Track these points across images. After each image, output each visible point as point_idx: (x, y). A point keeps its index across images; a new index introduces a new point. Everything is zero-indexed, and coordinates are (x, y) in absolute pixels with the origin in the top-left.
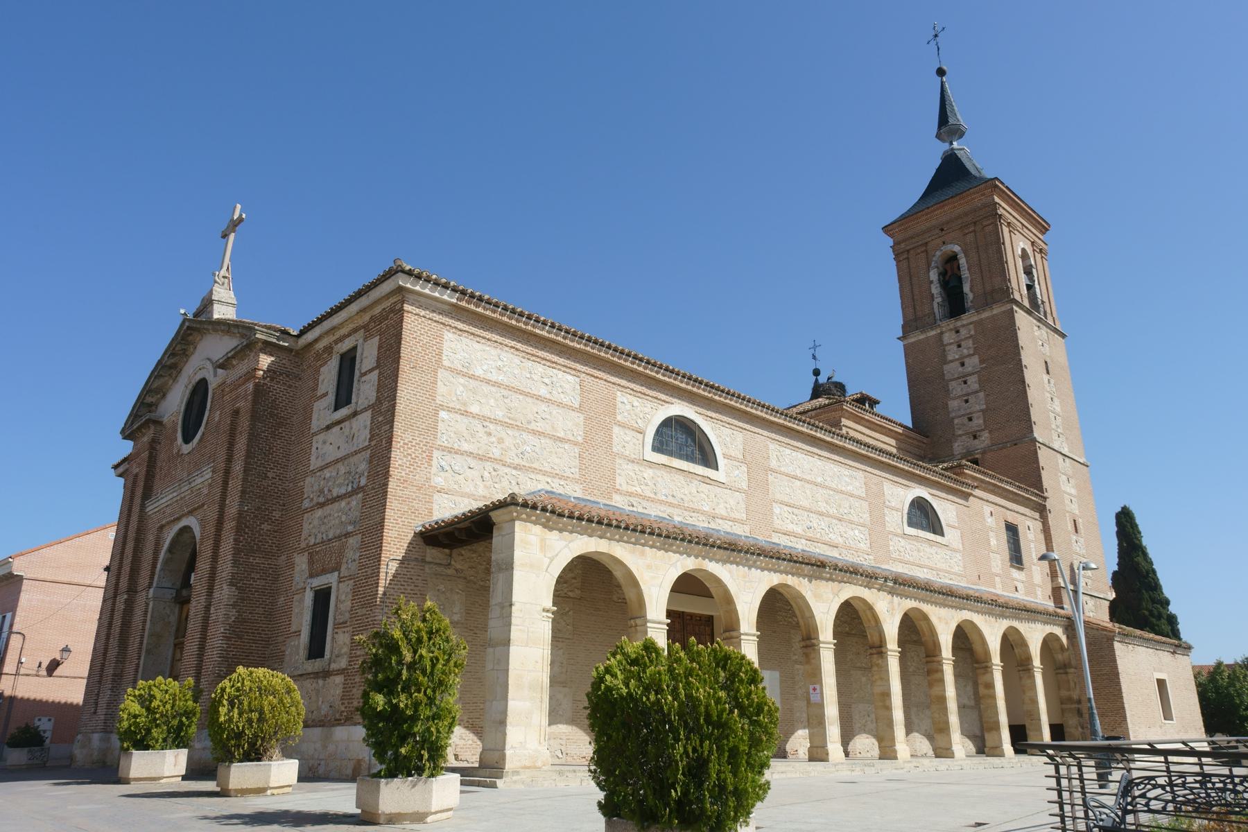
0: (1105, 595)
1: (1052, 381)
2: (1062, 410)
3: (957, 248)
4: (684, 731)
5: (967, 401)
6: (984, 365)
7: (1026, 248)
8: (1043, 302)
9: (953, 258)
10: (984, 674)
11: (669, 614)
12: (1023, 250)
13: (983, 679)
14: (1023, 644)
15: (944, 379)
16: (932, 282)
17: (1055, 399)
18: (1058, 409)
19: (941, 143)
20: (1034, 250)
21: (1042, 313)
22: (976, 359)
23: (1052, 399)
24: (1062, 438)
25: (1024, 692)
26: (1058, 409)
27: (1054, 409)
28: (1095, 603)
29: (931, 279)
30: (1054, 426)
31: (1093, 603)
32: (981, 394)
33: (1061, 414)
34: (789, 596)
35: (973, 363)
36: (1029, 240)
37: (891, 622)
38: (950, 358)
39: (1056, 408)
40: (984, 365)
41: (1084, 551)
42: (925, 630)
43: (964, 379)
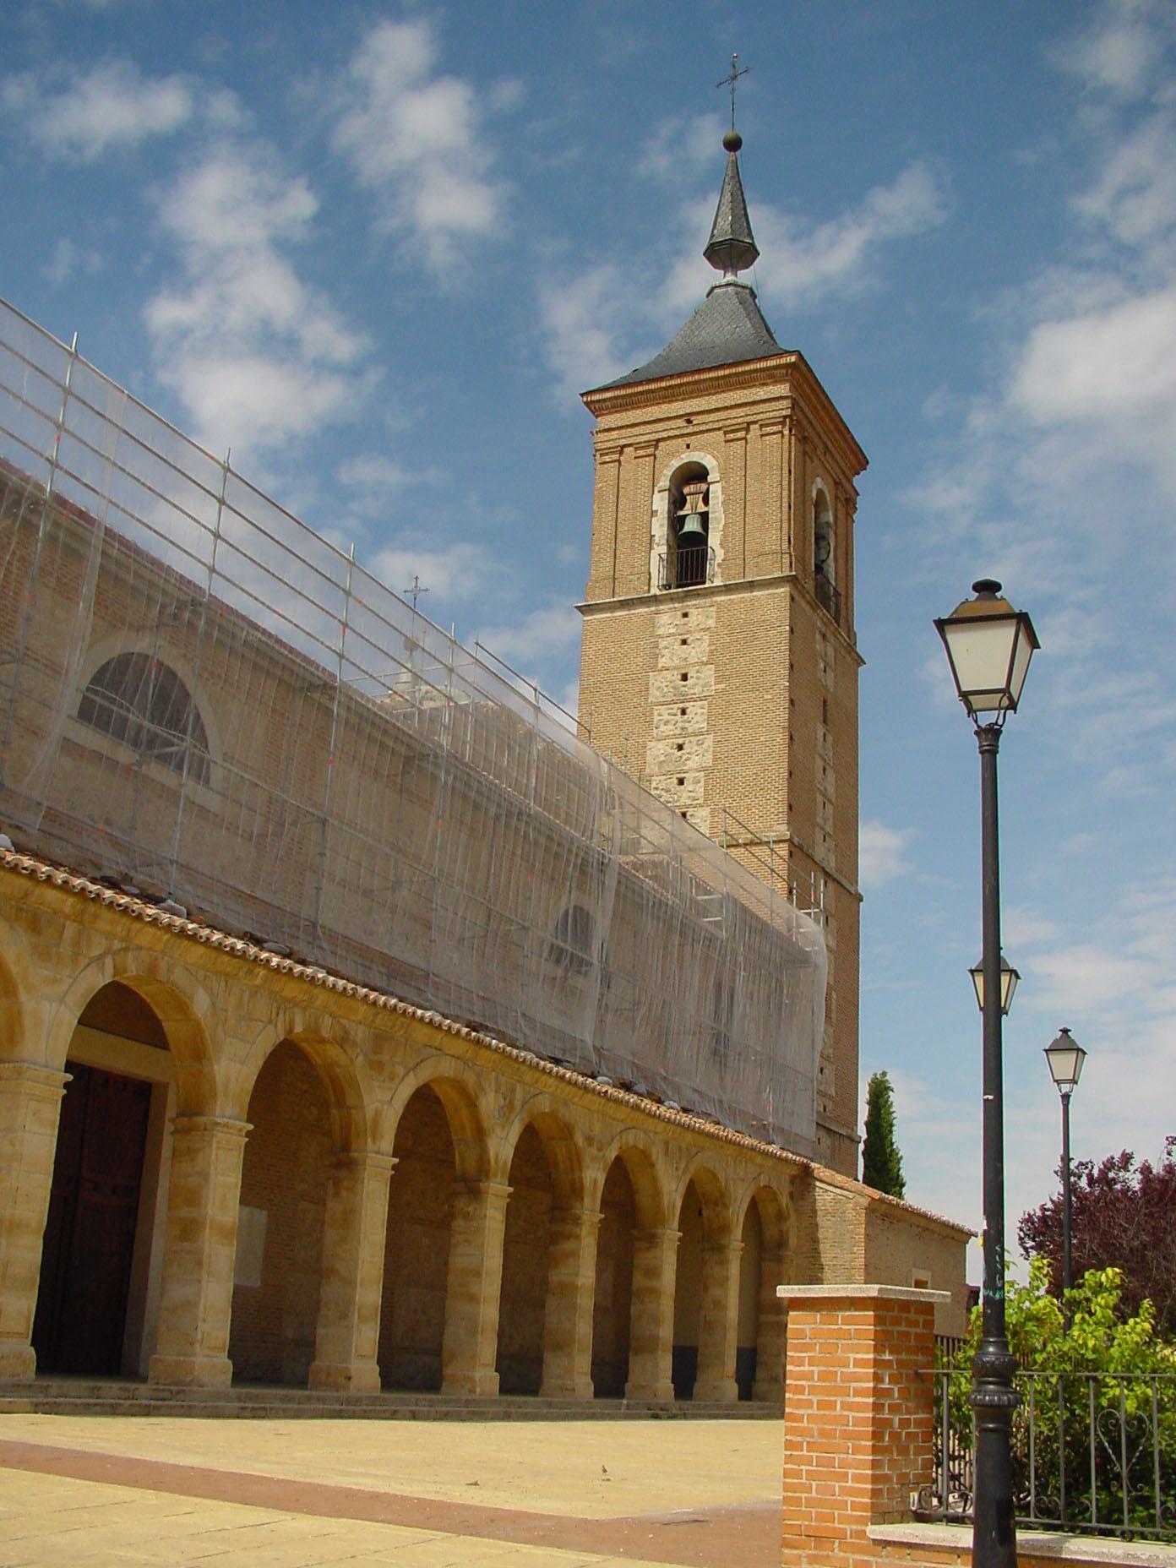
0: (850, 1131)
1: (830, 738)
2: (836, 793)
3: (709, 462)
4: (45, 523)
5: (680, 747)
6: (723, 686)
7: (826, 491)
8: (837, 594)
9: (695, 474)
10: (648, 1249)
11: (70, 1066)
12: (820, 492)
13: (643, 1259)
14: (720, 1200)
15: (717, 665)
16: (653, 513)
17: (829, 772)
18: (831, 790)
19: (711, 267)
20: (837, 497)
21: (832, 612)
22: (709, 671)
23: (824, 769)
24: (831, 843)
25: (706, 1288)
26: (831, 790)
27: (825, 789)
28: (833, 1143)
29: (654, 509)
30: (819, 820)
31: (829, 1143)
32: (709, 740)
33: (833, 800)
34: (317, 1059)
35: (704, 680)
36: (832, 476)
37: (504, 1135)
38: (662, 662)
39: (829, 788)
40: (723, 686)
41: (831, 1051)
42: (560, 1157)
43: (681, 705)
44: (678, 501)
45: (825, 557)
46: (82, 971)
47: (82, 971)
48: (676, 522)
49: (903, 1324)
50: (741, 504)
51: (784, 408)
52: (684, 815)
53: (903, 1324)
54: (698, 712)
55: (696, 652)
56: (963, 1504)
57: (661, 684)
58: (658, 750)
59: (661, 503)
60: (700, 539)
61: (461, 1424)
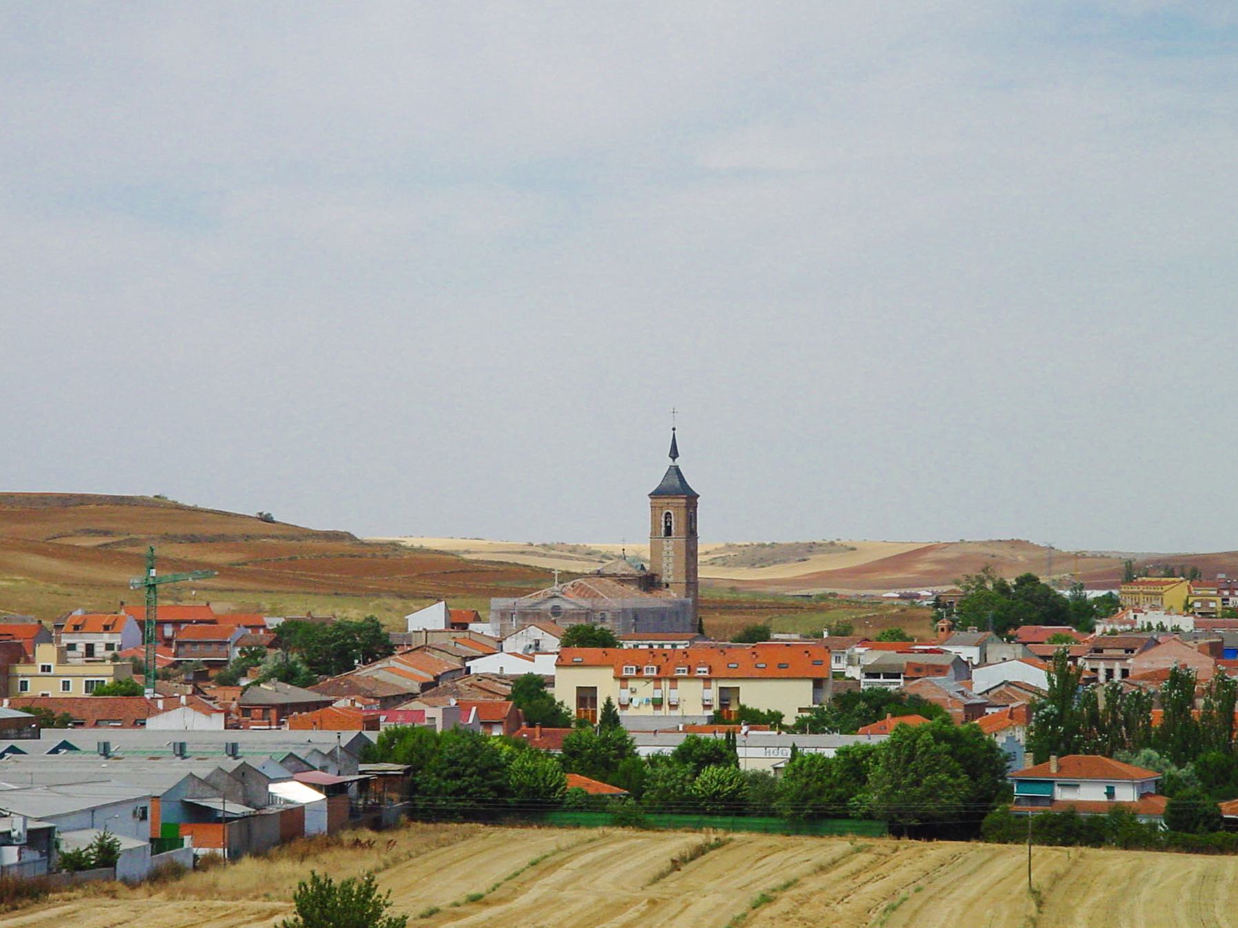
3: (671, 512)
9: (668, 513)
35: (672, 553)
44: (666, 518)
45: (19, 905)
46: (481, 552)
47: (481, 552)
48: (666, 523)
49: (882, 677)
50: (677, 522)
51: (684, 505)
52: (309, 741)
53: (882, 677)
54: (671, 559)
55: (670, 548)
56: (252, 711)
57: (664, 553)
58: (665, 565)
59: (663, 519)
60: (670, 527)
61: (1148, 853)
